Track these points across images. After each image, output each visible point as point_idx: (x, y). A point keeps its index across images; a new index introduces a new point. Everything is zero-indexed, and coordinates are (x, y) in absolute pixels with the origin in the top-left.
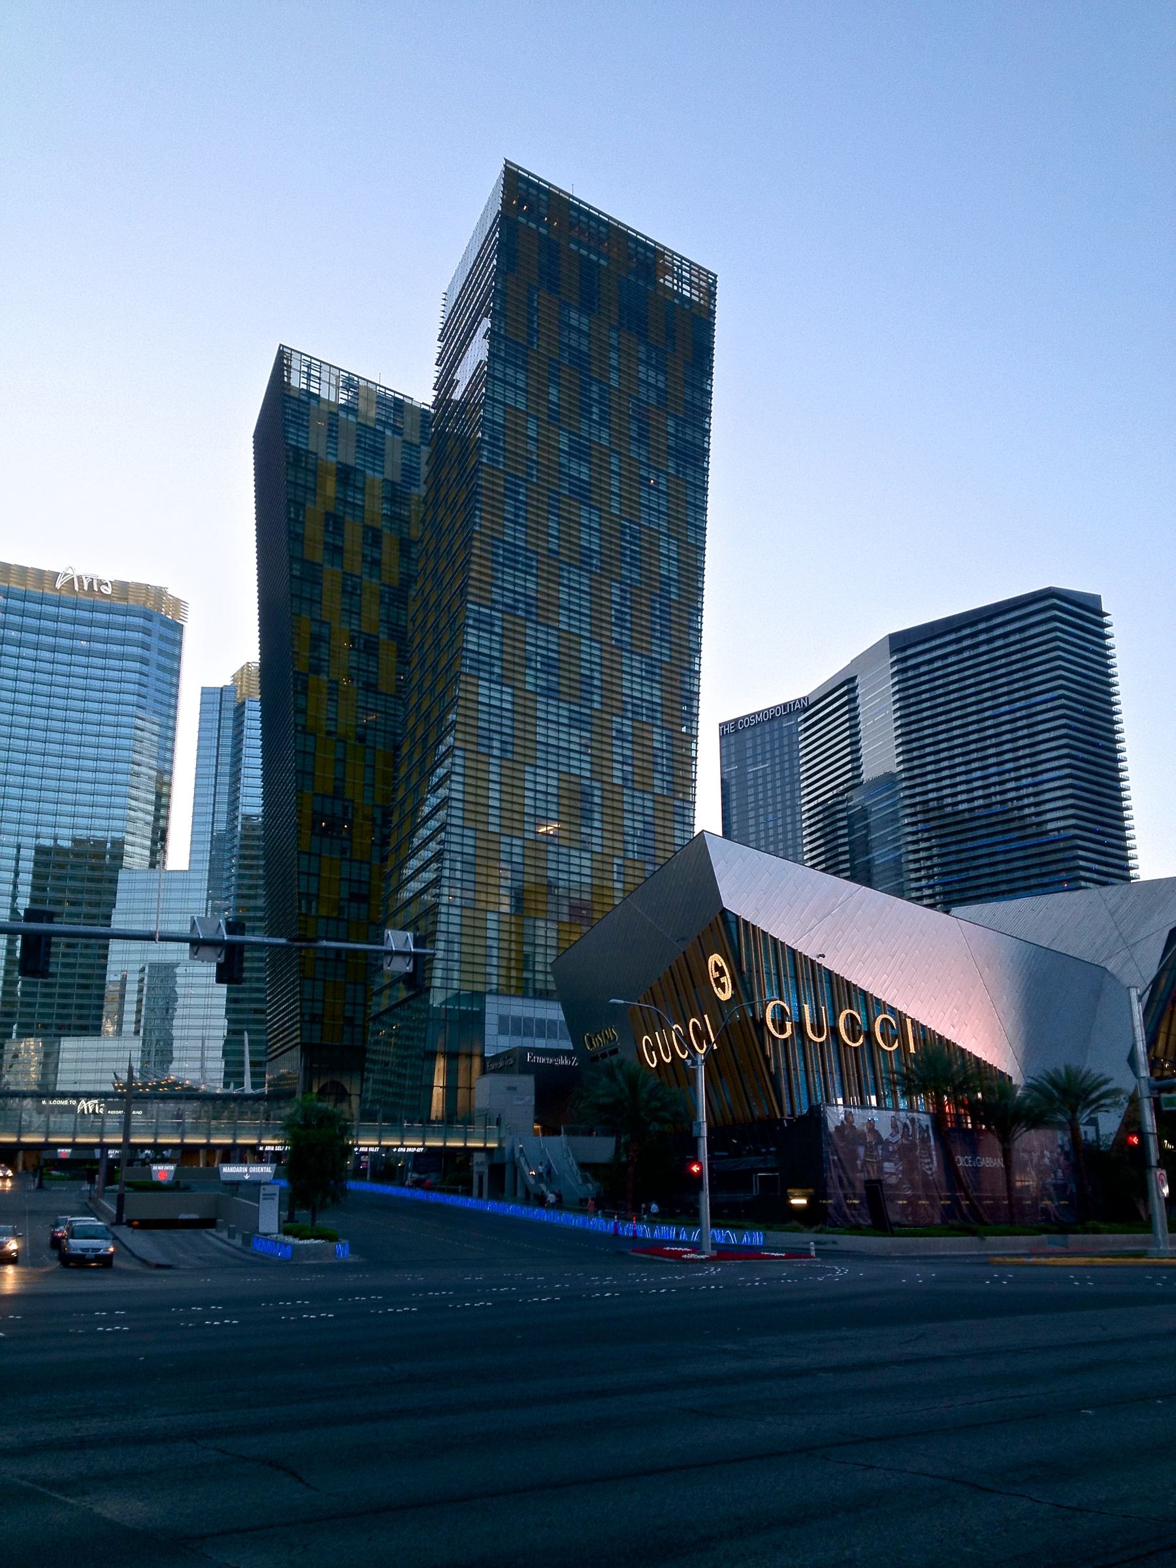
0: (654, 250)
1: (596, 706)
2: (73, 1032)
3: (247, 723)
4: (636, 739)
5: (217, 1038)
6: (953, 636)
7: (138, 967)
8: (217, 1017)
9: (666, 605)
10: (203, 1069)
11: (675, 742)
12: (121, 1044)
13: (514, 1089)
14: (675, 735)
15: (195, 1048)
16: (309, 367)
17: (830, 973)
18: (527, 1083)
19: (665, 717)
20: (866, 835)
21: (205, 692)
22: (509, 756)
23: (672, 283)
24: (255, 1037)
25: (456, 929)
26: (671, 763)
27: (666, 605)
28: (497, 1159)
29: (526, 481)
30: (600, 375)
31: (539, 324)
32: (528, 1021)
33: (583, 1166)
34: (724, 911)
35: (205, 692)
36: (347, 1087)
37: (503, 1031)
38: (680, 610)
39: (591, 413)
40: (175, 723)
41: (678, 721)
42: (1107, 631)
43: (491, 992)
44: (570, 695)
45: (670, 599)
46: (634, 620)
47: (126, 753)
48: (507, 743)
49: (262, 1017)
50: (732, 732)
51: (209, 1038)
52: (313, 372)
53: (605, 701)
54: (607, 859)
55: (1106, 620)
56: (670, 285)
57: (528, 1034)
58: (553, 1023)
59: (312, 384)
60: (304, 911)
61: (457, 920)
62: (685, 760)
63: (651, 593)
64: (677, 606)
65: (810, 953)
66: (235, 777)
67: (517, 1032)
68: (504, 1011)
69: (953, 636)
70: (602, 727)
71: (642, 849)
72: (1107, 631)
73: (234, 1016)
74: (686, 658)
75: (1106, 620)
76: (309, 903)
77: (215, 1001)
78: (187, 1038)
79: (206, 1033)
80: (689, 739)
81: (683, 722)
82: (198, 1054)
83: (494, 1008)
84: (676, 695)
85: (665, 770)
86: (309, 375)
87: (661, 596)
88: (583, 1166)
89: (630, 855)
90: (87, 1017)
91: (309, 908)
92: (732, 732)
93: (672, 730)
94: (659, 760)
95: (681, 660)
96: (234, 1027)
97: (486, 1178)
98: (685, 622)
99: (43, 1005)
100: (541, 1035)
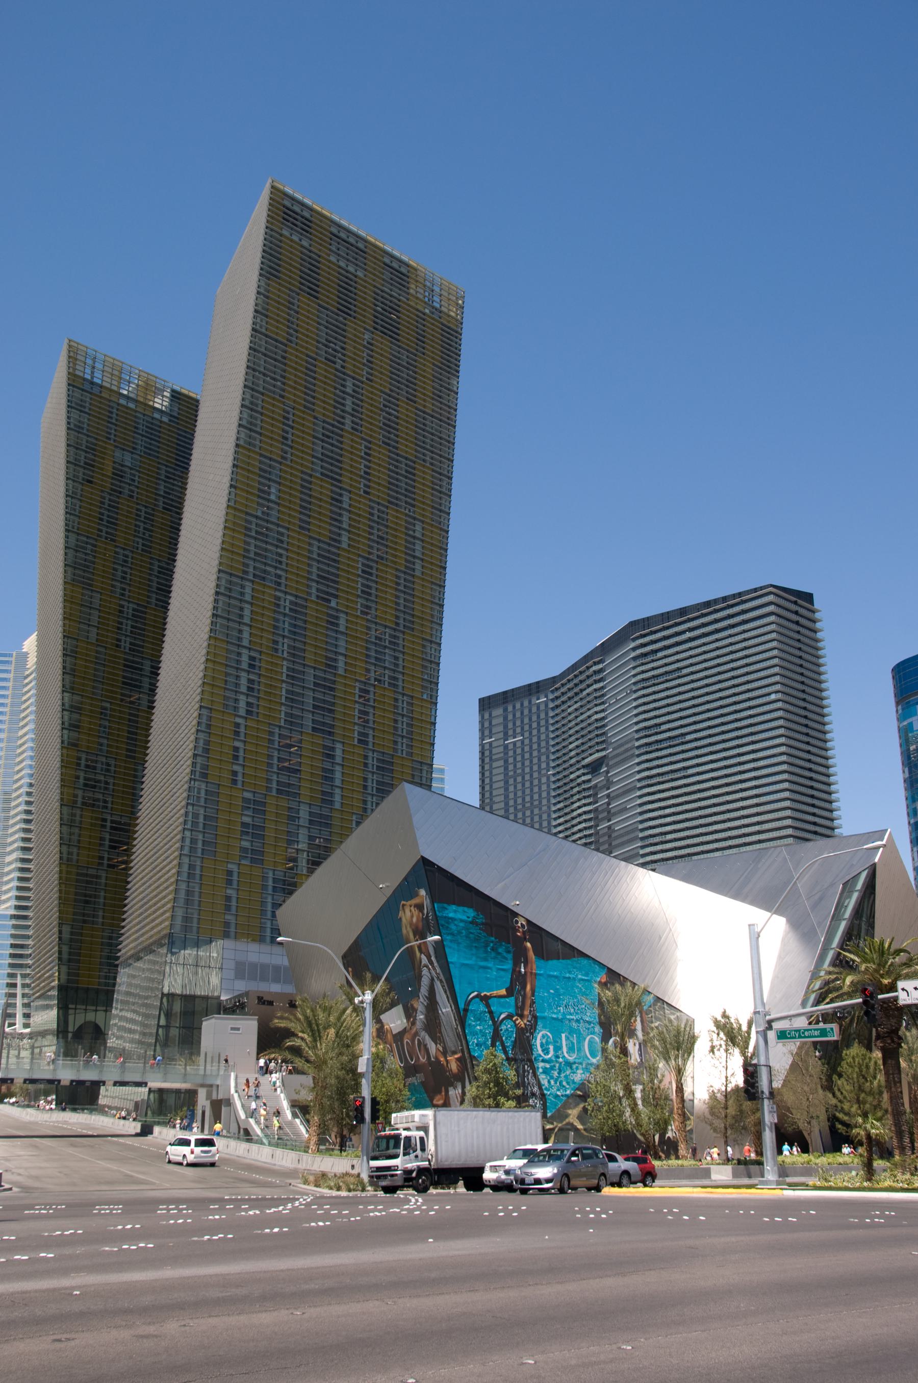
20: (608, 804)
27: (409, 581)
29: (280, 463)
30: (355, 354)
32: (264, 967)
57: (264, 979)
67: (253, 977)
100: (277, 980)
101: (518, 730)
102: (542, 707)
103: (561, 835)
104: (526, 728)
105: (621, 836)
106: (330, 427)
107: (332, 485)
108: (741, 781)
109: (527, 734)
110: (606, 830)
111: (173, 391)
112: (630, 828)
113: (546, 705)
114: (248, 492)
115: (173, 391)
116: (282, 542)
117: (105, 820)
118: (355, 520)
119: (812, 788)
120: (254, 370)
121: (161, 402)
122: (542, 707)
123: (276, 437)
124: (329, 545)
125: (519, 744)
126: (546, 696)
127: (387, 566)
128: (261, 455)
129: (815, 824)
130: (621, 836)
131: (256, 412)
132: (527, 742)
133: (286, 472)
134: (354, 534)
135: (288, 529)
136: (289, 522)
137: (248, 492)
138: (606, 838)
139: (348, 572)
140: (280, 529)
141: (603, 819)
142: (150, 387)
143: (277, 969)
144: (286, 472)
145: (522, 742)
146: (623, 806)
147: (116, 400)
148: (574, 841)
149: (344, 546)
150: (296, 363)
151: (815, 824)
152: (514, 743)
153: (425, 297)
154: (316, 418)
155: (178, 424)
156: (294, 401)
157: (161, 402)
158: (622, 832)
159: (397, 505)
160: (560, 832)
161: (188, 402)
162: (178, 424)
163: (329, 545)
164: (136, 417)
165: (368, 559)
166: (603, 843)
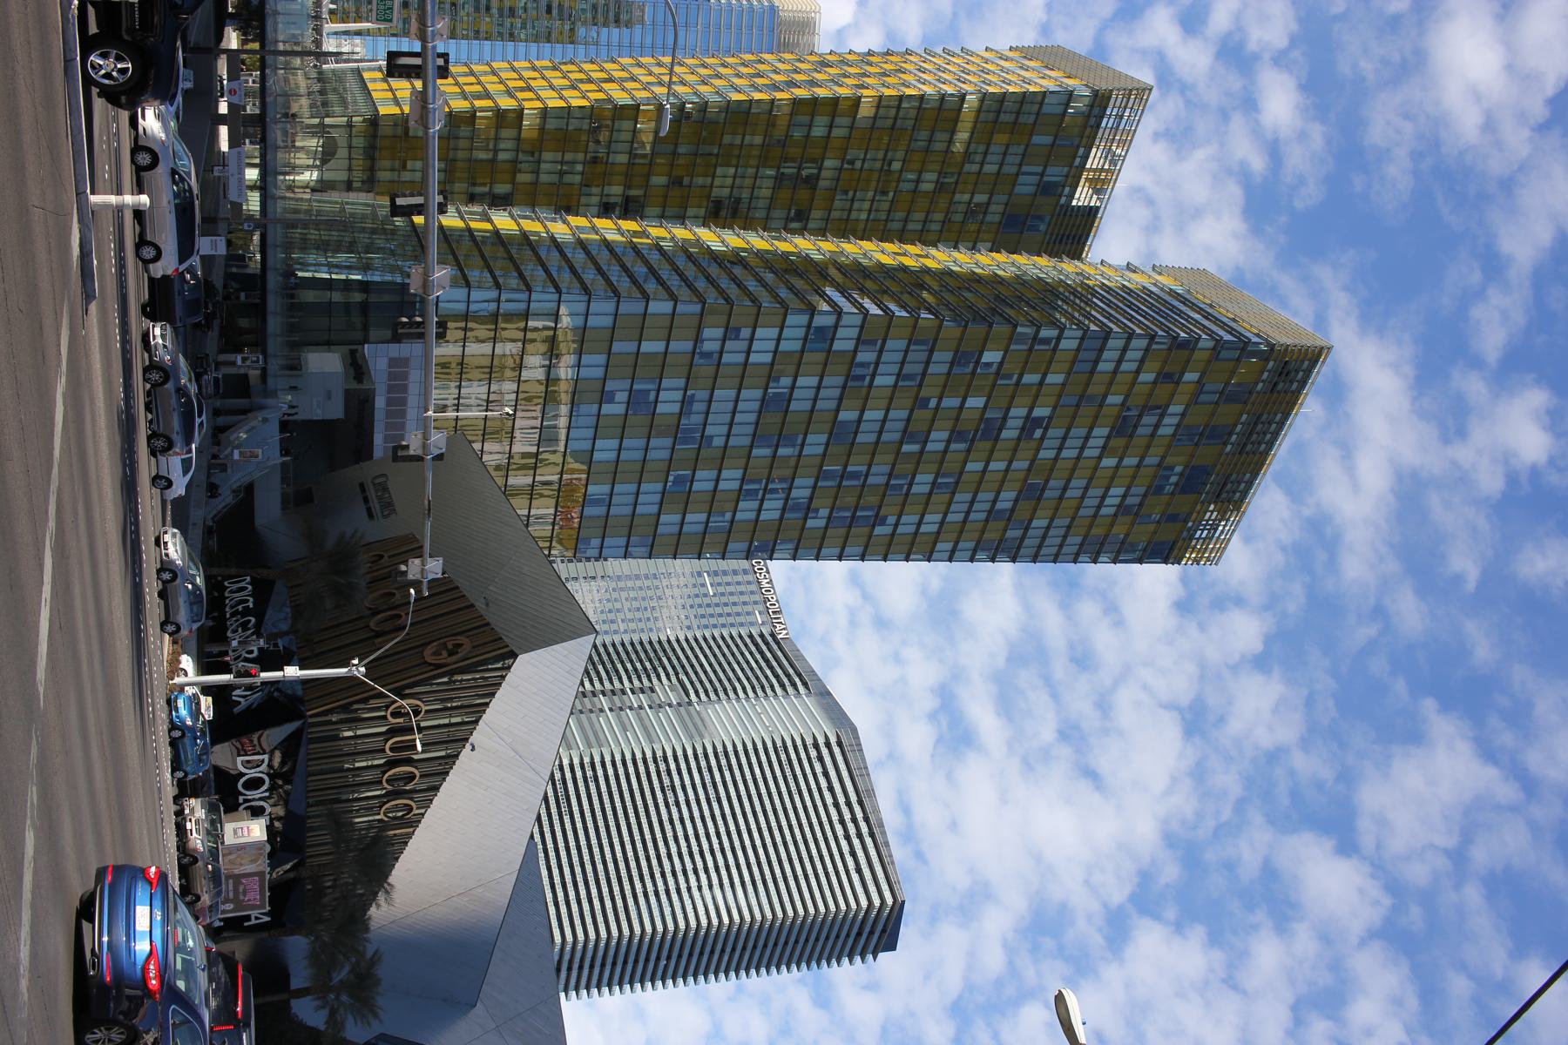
0: (1242, 500)
6: (853, 798)
17: (457, 756)
18: (336, 411)
20: (631, 708)
23: (1209, 519)
32: (404, 389)
33: (249, 489)
34: (514, 656)
37: (393, 362)
42: (701, 978)
55: (870, 957)
56: (1207, 517)
57: (391, 389)
65: (476, 737)
67: (392, 376)
69: (853, 798)
72: (701, 978)
75: (870, 957)
88: (249, 489)
100: (389, 402)
101: (721, 589)
102: (750, 619)
104: (724, 599)
105: (592, 724)
108: (775, 778)
109: (716, 600)
110: (599, 706)
111: (1098, 208)
112: (602, 737)
113: (752, 624)
115: (1098, 208)
119: (776, 944)
121: (1083, 196)
122: (750, 619)
125: (703, 590)
126: (763, 623)
129: (755, 947)
130: (592, 724)
132: (706, 601)
138: (589, 706)
141: (612, 701)
142: (1100, 185)
145: (706, 595)
146: (629, 727)
147: (1082, 144)
151: (755, 947)
152: (703, 585)
153: (1207, 521)
157: (1083, 196)
158: (597, 725)
161: (1085, 225)
166: (582, 704)
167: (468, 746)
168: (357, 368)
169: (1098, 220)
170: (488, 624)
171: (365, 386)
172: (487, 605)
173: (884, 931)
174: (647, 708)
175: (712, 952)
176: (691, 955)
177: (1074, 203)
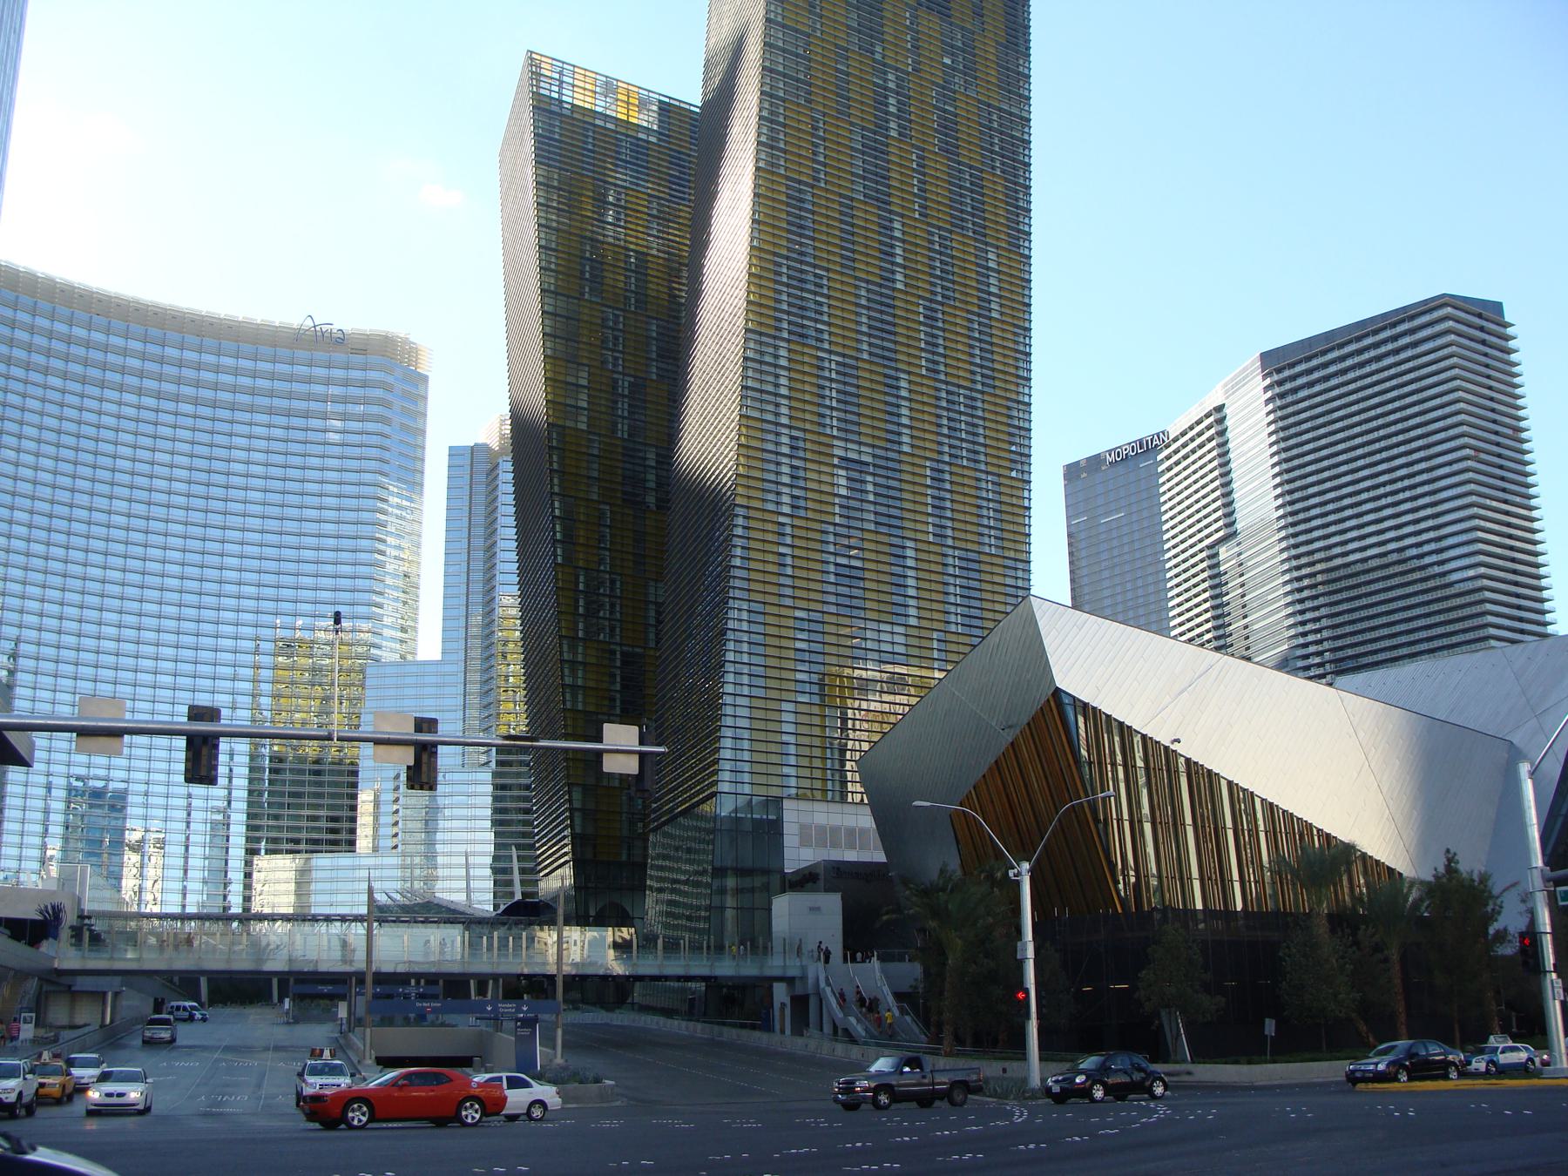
1: (913, 621)
2: (324, 847)
3: (500, 578)
4: (955, 488)
5: (483, 854)
7: (392, 774)
8: (483, 830)
9: (985, 325)
10: (468, 890)
11: (1005, 517)
12: (379, 861)
13: (818, 909)
14: (1003, 481)
15: (458, 866)
16: (561, 73)
18: (832, 904)
19: (989, 460)
21: (454, 452)
22: (801, 483)
24: (522, 853)
25: (744, 723)
26: (998, 516)
27: (985, 325)
28: (799, 991)
29: (813, 187)
30: (901, 157)
31: (825, 130)
32: (835, 830)
35: (454, 452)
36: (629, 909)
37: (805, 841)
38: (1005, 356)
39: (887, 105)
40: (423, 454)
41: (1007, 464)
43: (789, 797)
44: (872, 390)
45: (990, 318)
46: (949, 370)
47: (371, 502)
48: (798, 497)
49: (529, 829)
50: (1073, 472)
51: (474, 854)
52: (565, 79)
53: (914, 387)
54: (924, 633)
55: (1510, 331)
57: (835, 845)
58: (863, 831)
59: (564, 91)
60: (569, 705)
61: (745, 712)
62: (1016, 510)
63: (968, 311)
64: (999, 325)
66: (490, 551)
67: (822, 843)
68: (806, 819)
70: (914, 474)
71: (964, 564)
73: (500, 829)
74: (1013, 388)
76: (574, 696)
77: (479, 812)
78: (450, 854)
79: (470, 848)
80: (1020, 485)
81: (1013, 466)
82: (463, 872)
83: (793, 815)
84: (1002, 423)
85: (991, 496)
86: (562, 82)
87: (979, 315)
89: (953, 628)
90: (340, 807)
91: (575, 677)
92: (1073, 472)
93: (999, 475)
94: (985, 512)
95: (1006, 390)
96: (500, 841)
97: (788, 1011)
98: (1011, 345)
99: (293, 783)
100: (852, 846)
103: (1184, 638)
106: (878, 298)
107: (879, 208)
114: (774, 226)
116: (821, 286)
117: (613, 652)
118: (910, 252)
120: (771, 96)
123: (805, 179)
124: (881, 286)
127: (956, 308)
128: (788, 178)
130: (1253, 372)
131: (779, 123)
133: (820, 197)
134: (911, 243)
135: (828, 270)
136: (828, 234)
137: (774, 226)
139: (909, 346)
140: (819, 326)
143: (851, 832)
144: (820, 197)
148: (1202, 645)
149: (899, 286)
150: (843, 291)
154: (852, 124)
155: (669, 143)
156: (823, 56)
159: (963, 228)
160: (1181, 634)
161: (680, 114)
162: (669, 143)
163: (881, 286)
164: (617, 139)
165: (931, 301)
167: (1173, 747)
168: (805, 880)
169: (682, 105)
170: (1029, 724)
171: (821, 871)
172: (1010, 727)
173: (1480, 316)
174: (1246, 620)
175: (1512, 548)
176: (1516, 584)
177: (655, 127)
